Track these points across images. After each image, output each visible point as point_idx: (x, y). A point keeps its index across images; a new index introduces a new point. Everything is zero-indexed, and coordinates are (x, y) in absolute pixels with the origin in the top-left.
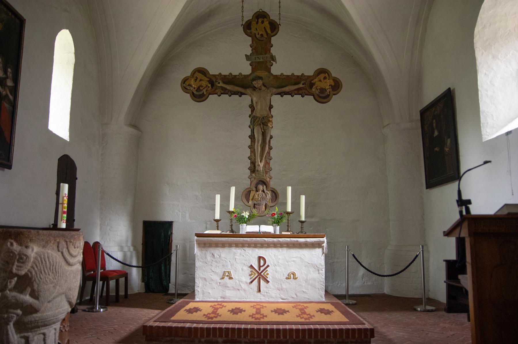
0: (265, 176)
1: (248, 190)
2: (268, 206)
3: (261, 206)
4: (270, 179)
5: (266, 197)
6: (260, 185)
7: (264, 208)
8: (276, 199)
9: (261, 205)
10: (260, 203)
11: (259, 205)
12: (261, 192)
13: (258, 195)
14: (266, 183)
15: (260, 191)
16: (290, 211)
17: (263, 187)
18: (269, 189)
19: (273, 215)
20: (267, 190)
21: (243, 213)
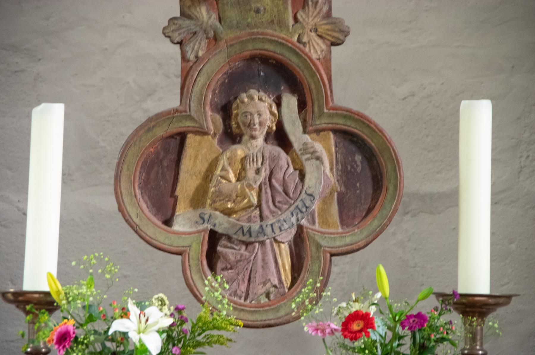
0: (291, 22)
1: (161, 132)
2: (319, 246)
3: (264, 253)
4: (333, 44)
5: (302, 176)
6: (253, 92)
7: (286, 261)
8: (375, 199)
9: (262, 243)
10: (255, 227)
11: (247, 244)
12: (260, 141)
13: (243, 168)
14: (304, 75)
15: (253, 137)
16: (486, 290)
17: (279, 105)
18: (322, 123)
19: (356, 326)
20: (305, 132)
21: (125, 314)
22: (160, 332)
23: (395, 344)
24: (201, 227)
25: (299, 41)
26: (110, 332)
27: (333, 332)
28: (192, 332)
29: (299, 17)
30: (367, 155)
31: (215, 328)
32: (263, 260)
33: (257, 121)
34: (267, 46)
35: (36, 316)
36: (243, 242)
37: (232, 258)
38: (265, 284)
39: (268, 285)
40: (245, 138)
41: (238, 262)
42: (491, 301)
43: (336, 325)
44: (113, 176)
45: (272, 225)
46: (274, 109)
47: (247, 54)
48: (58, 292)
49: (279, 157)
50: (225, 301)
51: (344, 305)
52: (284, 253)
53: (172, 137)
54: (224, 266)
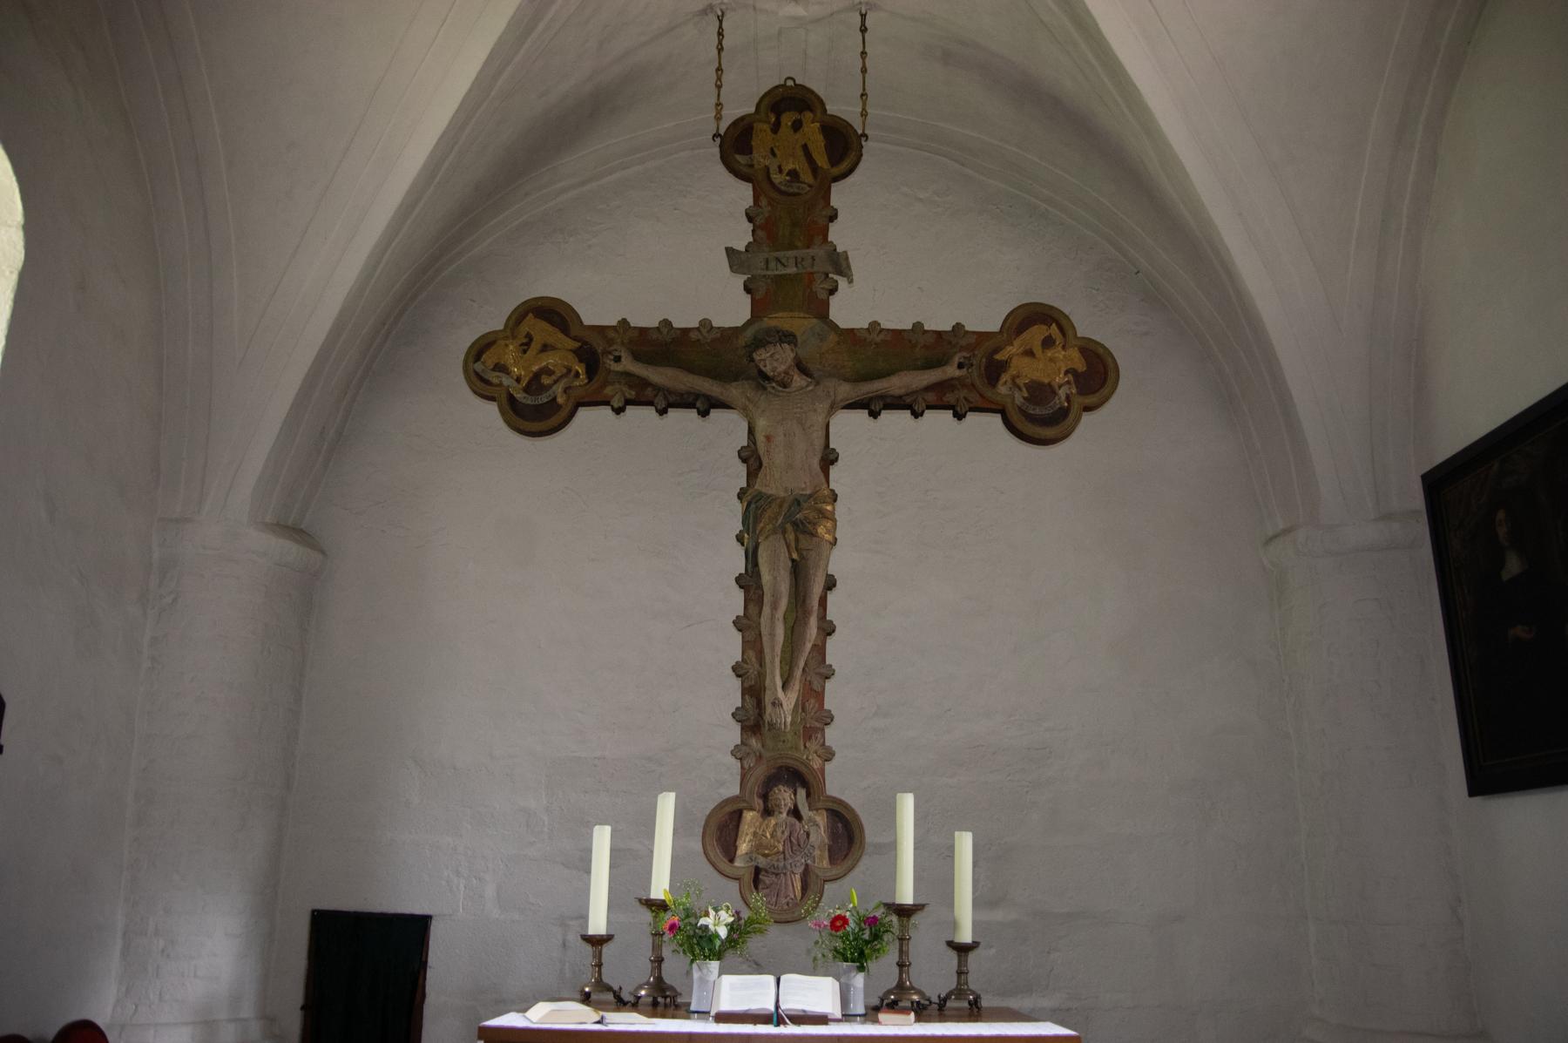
0: (802, 748)
1: (728, 809)
2: (817, 876)
3: (786, 880)
4: (826, 760)
6: (781, 787)
7: (798, 885)
9: (785, 874)
10: (781, 864)
11: (777, 875)
12: (785, 815)
14: (810, 778)
15: (781, 813)
17: (795, 794)
18: (820, 805)
19: (838, 923)
21: (707, 914)
22: (726, 925)
23: (860, 934)
24: (750, 864)
25: (807, 758)
26: (699, 925)
27: (825, 926)
28: (745, 925)
29: (807, 745)
30: (819, 736)
31: (757, 923)
32: (785, 883)
33: (783, 803)
34: (788, 761)
35: (657, 913)
36: (774, 873)
37: (767, 882)
38: (786, 898)
39: (788, 898)
40: (776, 813)
41: (771, 884)
42: (914, 908)
43: (826, 923)
44: (843, 798)
45: (791, 864)
46: (792, 796)
47: (778, 765)
48: (670, 901)
49: (795, 824)
50: (764, 908)
51: (831, 911)
52: (797, 880)
53: (734, 812)
54: (742, 915)
